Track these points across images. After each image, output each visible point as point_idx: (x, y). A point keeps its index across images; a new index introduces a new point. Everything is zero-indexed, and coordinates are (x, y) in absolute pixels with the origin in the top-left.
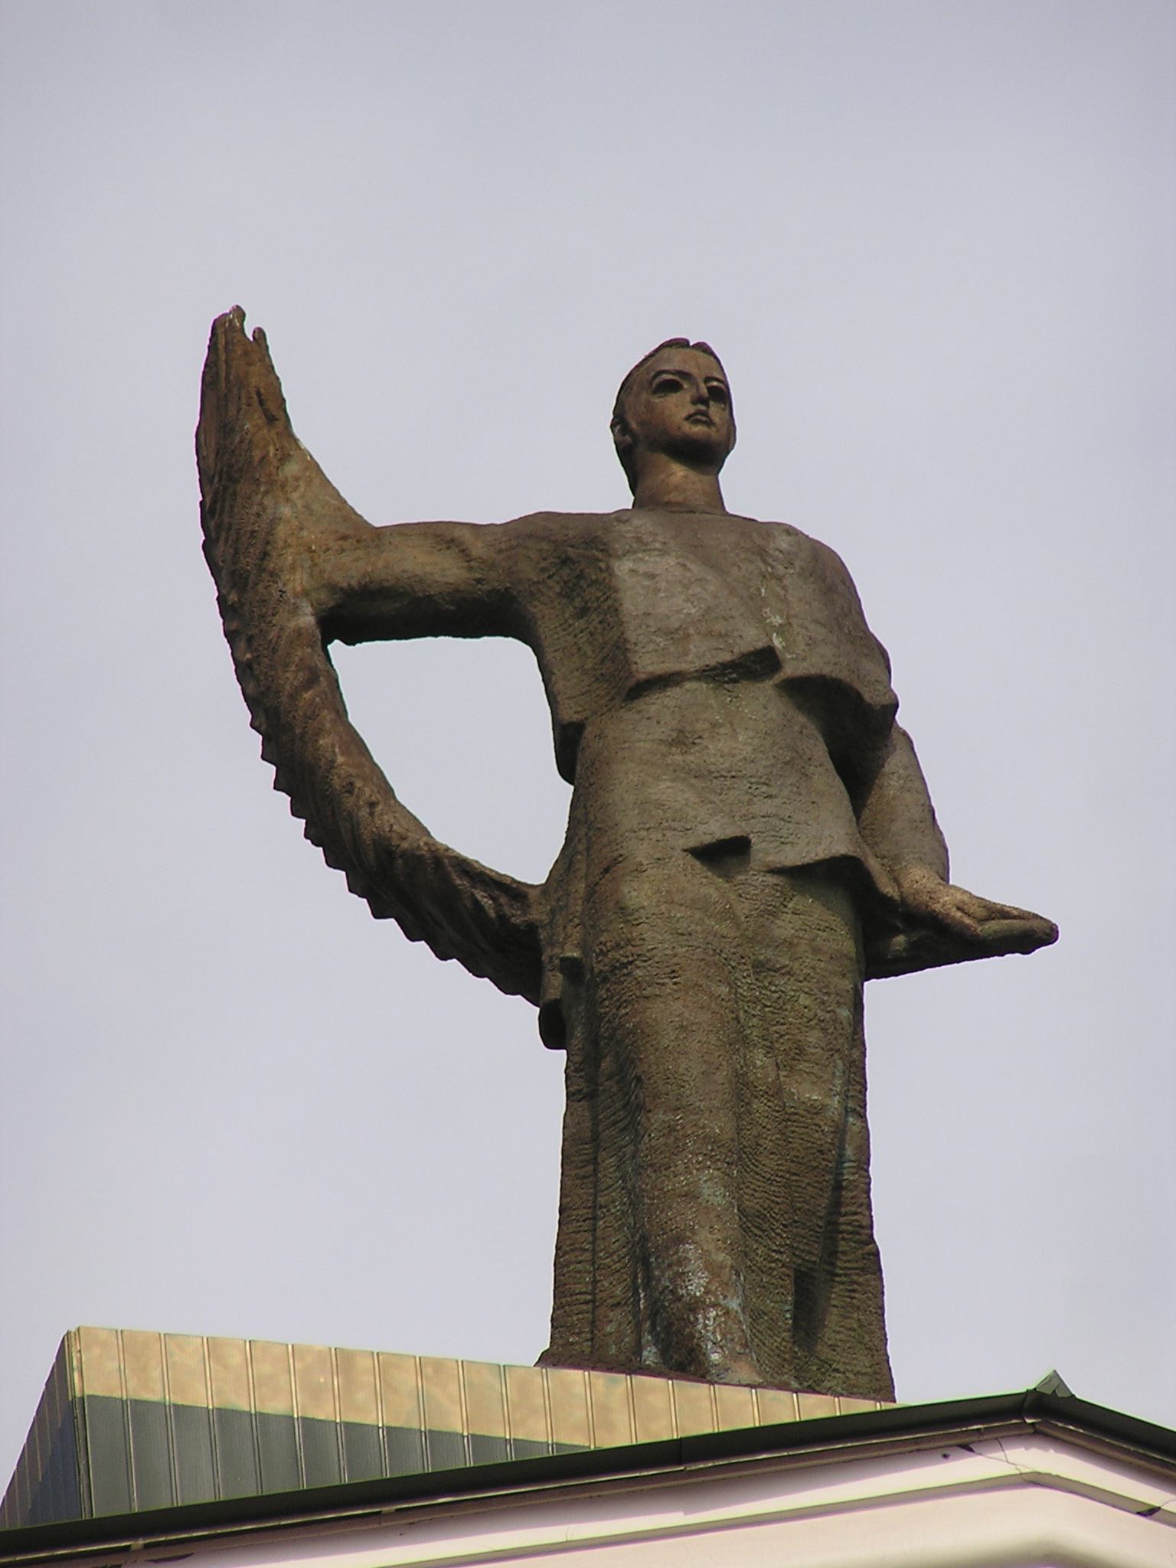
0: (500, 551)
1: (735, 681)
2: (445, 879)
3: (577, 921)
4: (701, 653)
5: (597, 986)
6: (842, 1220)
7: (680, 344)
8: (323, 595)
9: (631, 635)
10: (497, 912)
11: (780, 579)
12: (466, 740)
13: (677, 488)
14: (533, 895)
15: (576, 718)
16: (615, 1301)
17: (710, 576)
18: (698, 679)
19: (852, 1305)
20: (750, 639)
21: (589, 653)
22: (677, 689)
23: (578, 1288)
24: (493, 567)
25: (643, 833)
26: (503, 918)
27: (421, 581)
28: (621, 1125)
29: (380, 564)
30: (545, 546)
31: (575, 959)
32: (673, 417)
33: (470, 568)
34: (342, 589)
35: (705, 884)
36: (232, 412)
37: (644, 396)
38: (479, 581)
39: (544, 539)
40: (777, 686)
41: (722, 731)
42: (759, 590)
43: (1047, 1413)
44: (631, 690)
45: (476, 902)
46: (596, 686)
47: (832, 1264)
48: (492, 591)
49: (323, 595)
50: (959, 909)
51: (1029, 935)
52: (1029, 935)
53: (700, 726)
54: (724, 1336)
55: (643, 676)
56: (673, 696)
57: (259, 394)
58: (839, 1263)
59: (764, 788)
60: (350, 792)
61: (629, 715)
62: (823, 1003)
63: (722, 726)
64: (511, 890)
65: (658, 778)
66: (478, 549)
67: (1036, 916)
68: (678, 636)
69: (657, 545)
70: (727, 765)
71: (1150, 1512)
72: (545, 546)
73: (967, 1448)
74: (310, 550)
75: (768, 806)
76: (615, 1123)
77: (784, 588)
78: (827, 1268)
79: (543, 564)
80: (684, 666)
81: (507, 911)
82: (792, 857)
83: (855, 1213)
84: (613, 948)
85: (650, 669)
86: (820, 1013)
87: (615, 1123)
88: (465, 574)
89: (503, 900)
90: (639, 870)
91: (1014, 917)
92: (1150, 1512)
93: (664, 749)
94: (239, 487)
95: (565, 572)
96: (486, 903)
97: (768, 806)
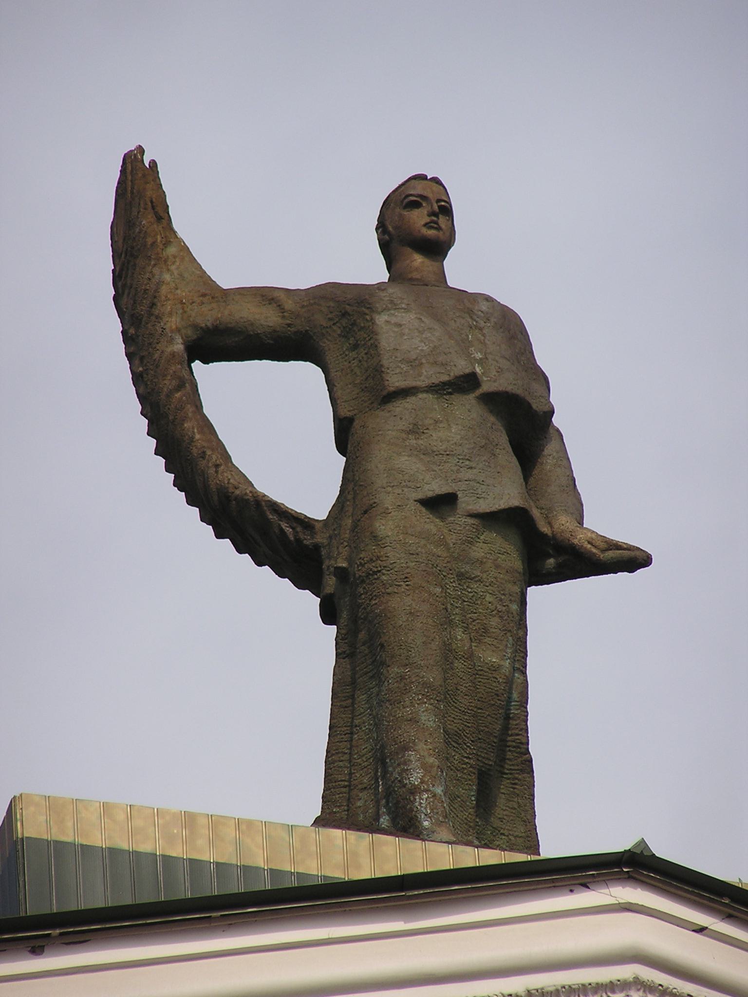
0: (303, 307)
1: (450, 394)
2: (262, 514)
3: (346, 544)
4: (430, 375)
6: (509, 738)
7: (422, 177)
8: (189, 332)
9: (385, 362)
10: (295, 537)
11: (481, 329)
13: (417, 269)
14: (318, 526)
15: (349, 414)
16: (365, 785)
18: (427, 392)
19: (514, 793)
20: (461, 367)
22: (414, 398)
23: (340, 777)
25: (390, 489)
26: (298, 541)
27: (252, 324)
29: (226, 313)
30: (332, 304)
31: (344, 568)
32: (416, 223)
33: (283, 317)
34: (201, 328)
35: (428, 523)
37: (398, 210)
38: (289, 325)
40: (477, 397)
41: (441, 425)
43: (637, 865)
44: (385, 397)
45: (282, 530)
47: (502, 767)
48: (295, 332)
49: (189, 332)
50: (589, 543)
51: (633, 561)
52: (633, 561)
53: (428, 422)
54: (432, 810)
55: (392, 389)
56: (411, 402)
57: (152, 202)
58: (507, 766)
59: (467, 463)
60: (203, 458)
62: (501, 600)
63: (441, 422)
65: (399, 454)
66: (289, 305)
68: (415, 364)
70: (444, 447)
71: (701, 930)
72: (332, 304)
73: (586, 886)
74: (182, 303)
75: (470, 474)
76: (366, 673)
77: (484, 335)
79: (330, 316)
80: (414, 384)
81: (302, 536)
82: (484, 506)
84: (368, 562)
85: (397, 384)
86: (499, 607)
87: (366, 673)
88: (280, 320)
89: (299, 529)
91: (625, 549)
92: (701, 930)
93: (404, 435)
95: (344, 322)
96: (288, 530)
97: (470, 474)
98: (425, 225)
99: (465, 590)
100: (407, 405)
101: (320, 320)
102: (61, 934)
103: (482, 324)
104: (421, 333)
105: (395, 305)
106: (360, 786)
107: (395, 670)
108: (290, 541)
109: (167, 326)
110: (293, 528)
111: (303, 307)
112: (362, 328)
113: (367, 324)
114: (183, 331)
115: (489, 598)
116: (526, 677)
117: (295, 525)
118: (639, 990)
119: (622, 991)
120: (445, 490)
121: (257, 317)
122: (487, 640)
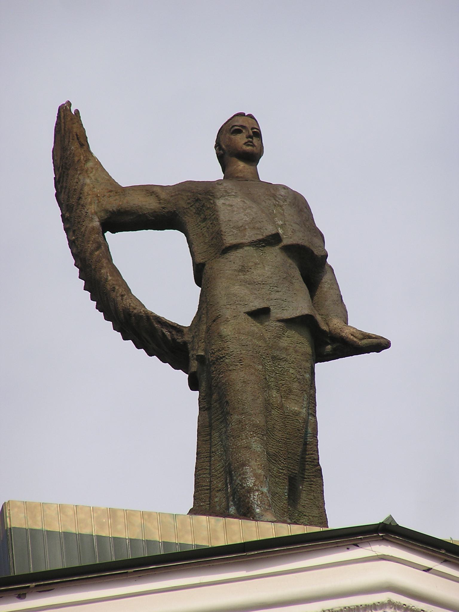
0: (172, 196)
1: (264, 246)
2: (151, 325)
4: (251, 236)
6: (307, 456)
7: (242, 115)
8: (103, 214)
9: (223, 229)
10: (171, 338)
11: (281, 206)
12: (159, 271)
13: (241, 171)
15: (202, 261)
18: (249, 246)
19: (311, 490)
20: (270, 230)
23: (204, 484)
24: (169, 202)
25: (229, 306)
26: (174, 340)
27: (141, 208)
28: (221, 420)
29: (125, 201)
31: (202, 355)
32: (239, 143)
33: (160, 203)
35: (253, 326)
36: (66, 143)
37: (228, 135)
38: (163, 208)
39: (189, 191)
41: (259, 266)
42: (273, 211)
43: (388, 531)
44: (224, 250)
45: (163, 333)
47: (304, 474)
48: (168, 212)
49: (103, 214)
50: (352, 335)
51: (379, 345)
52: (379, 345)
54: (261, 502)
55: (228, 245)
56: (239, 253)
57: (77, 135)
58: (306, 474)
59: (276, 288)
60: (114, 291)
61: (222, 260)
62: (299, 372)
63: (259, 264)
64: (177, 329)
65: (234, 285)
66: (163, 195)
67: (382, 338)
68: (241, 229)
70: (261, 279)
71: (428, 570)
73: (356, 545)
74: (97, 196)
75: (277, 296)
77: (283, 210)
78: (301, 475)
79: (188, 201)
80: (242, 241)
81: (175, 337)
83: (312, 454)
84: (217, 351)
85: (231, 242)
86: (298, 376)
88: (158, 206)
91: (374, 338)
92: (428, 570)
93: (236, 273)
95: (197, 204)
96: (167, 334)
97: (277, 296)
98: (245, 144)
99: (277, 366)
101: (182, 204)
102: (36, 586)
103: (282, 203)
105: (229, 193)
107: (236, 417)
109: (89, 211)
110: (169, 332)
112: (208, 208)
114: (99, 214)
115: (291, 371)
116: (316, 418)
117: (171, 330)
118: (391, 608)
119: (381, 609)
120: (263, 305)
121: (144, 203)
122: (291, 396)
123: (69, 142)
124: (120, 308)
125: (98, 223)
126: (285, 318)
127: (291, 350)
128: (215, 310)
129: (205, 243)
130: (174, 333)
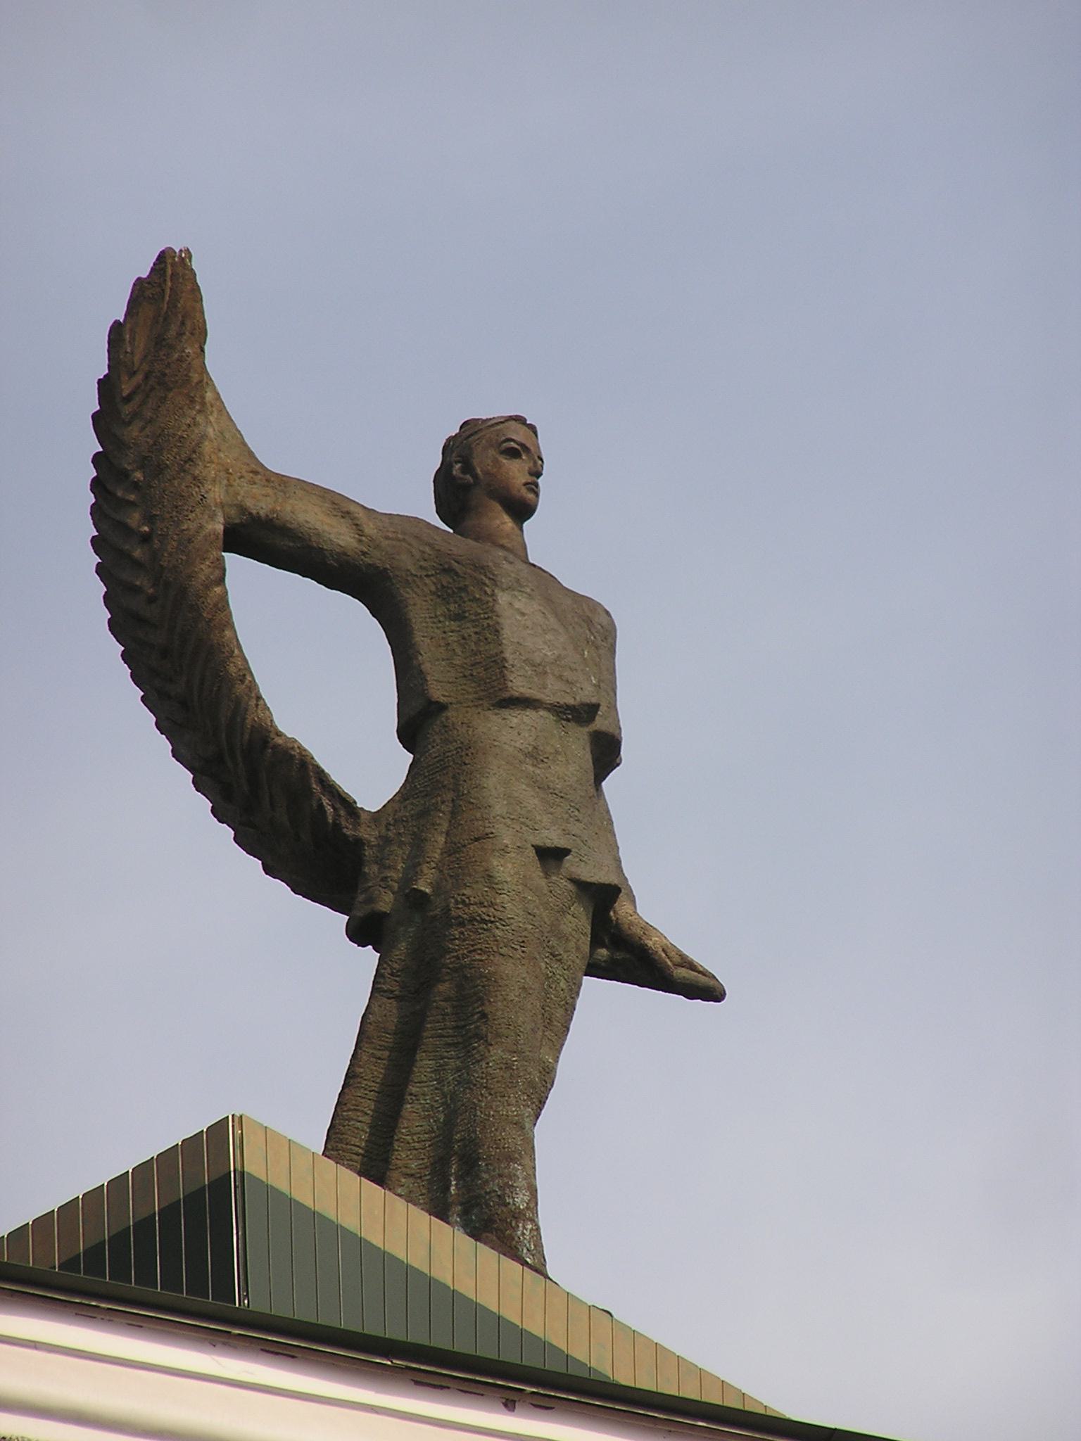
0: (387, 538)
1: (568, 720)
4: (553, 692)
5: (451, 926)
7: (520, 420)
8: (233, 512)
9: (507, 655)
13: (508, 536)
14: (363, 816)
15: (442, 700)
16: (409, 1172)
17: (561, 630)
18: (549, 710)
21: (458, 651)
22: (534, 713)
23: (354, 1141)
24: (377, 547)
25: (509, 822)
26: (337, 826)
27: (318, 535)
28: (449, 1040)
29: (289, 508)
31: (425, 894)
32: (486, 475)
33: (360, 541)
34: (250, 514)
36: (172, 332)
37: (492, 452)
38: (364, 553)
39: (429, 545)
44: (504, 700)
45: (321, 806)
46: (463, 681)
49: (233, 512)
51: (709, 991)
52: (709, 991)
60: (242, 682)
61: (494, 718)
64: (346, 804)
66: (370, 529)
68: (540, 669)
69: (528, 590)
72: (427, 549)
74: (227, 471)
76: (441, 1036)
77: (599, 656)
79: (422, 563)
80: (539, 696)
81: (344, 823)
84: (475, 904)
85: (522, 690)
87: (441, 1036)
88: (354, 544)
89: (342, 813)
90: (504, 850)
91: (700, 972)
94: (171, 395)
95: (445, 579)
96: (329, 809)
98: (525, 484)
100: (525, 719)
101: (406, 562)
102: (533, 1393)
103: (599, 642)
104: (545, 632)
105: (522, 586)
106: (404, 1170)
107: (497, 1053)
108: (327, 823)
109: (210, 496)
110: (333, 807)
111: (387, 538)
113: (485, 598)
117: (338, 806)
120: (562, 843)
121: (326, 528)
123: (181, 334)
124: (249, 722)
125: (220, 528)
126: (583, 879)
127: (572, 944)
128: (483, 819)
129: (453, 666)
130: (342, 813)
